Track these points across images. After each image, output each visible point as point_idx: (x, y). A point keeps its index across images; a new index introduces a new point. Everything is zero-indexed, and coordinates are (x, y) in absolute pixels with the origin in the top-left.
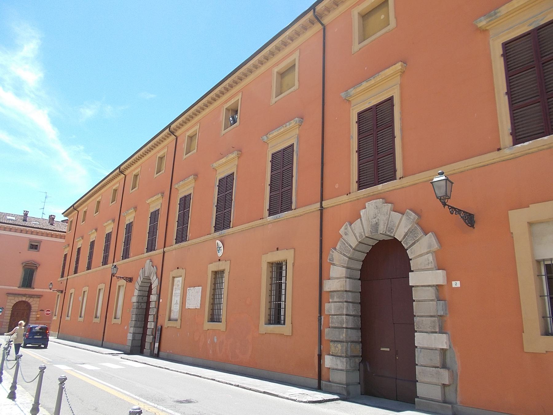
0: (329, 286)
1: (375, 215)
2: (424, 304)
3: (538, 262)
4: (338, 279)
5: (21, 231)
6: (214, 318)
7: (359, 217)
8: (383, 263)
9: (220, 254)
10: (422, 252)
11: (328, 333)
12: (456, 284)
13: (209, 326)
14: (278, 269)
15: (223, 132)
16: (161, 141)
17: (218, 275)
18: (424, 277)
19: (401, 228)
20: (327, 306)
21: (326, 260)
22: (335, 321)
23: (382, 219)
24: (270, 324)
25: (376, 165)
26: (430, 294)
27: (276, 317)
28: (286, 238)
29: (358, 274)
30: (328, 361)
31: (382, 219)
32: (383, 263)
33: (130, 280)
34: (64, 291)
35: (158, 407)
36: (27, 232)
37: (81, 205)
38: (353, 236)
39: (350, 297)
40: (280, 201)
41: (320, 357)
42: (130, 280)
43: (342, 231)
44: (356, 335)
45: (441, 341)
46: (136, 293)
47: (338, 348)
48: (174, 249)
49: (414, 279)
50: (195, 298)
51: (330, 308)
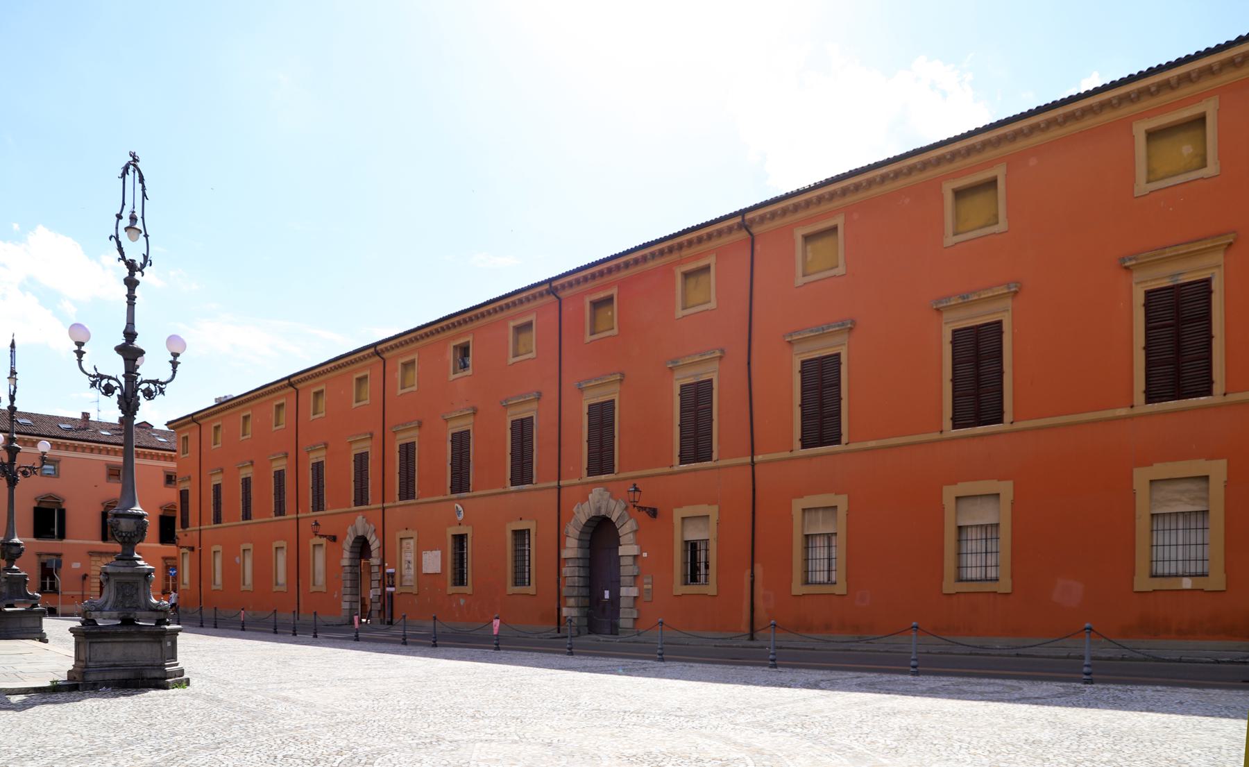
0: (566, 554)
1: (598, 499)
2: (627, 569)
3: (686, 542)
4: (571, 549)
5: (92, 450)
6: (460, 579)
7: (587, 499)
8: (600, 532)
9: (460, 518)
10: (626, 530)
11: (564, 591)
12: (645, 555)
13: (452, 589)
14: (520, 536)
15: (452, 377)
16: (361, 359)
17: (460, 540)
18: (627, 549)
19: (615, 511)
20: (564, 570)
21: (563, 532)
22: (569, 582)
23: (604, 504)
24: (686, 584)
25: (601, 461)
26: (630, 561)
27: (519, 580)
28: (529, 507)
29: (587, 544)
30: (565, 612)
31: (604, 504)
32: (600, 532)
33: (334, 539)
34: (197, 549)
35: (703, 559)
36: (100, 451)
37: (208, 416)
38: (583, 513)
39: (581, 563)
40: (522, 473)
41: (559, 609)
42: (334, 539)
43: (575, 510)
44: (585, 592)
45: (634, 592)
46: (347, 554)
47: (571, 602)
48: (398, 509)
49: (622, 551)
50: (433, 562)
51: (566, 571)
